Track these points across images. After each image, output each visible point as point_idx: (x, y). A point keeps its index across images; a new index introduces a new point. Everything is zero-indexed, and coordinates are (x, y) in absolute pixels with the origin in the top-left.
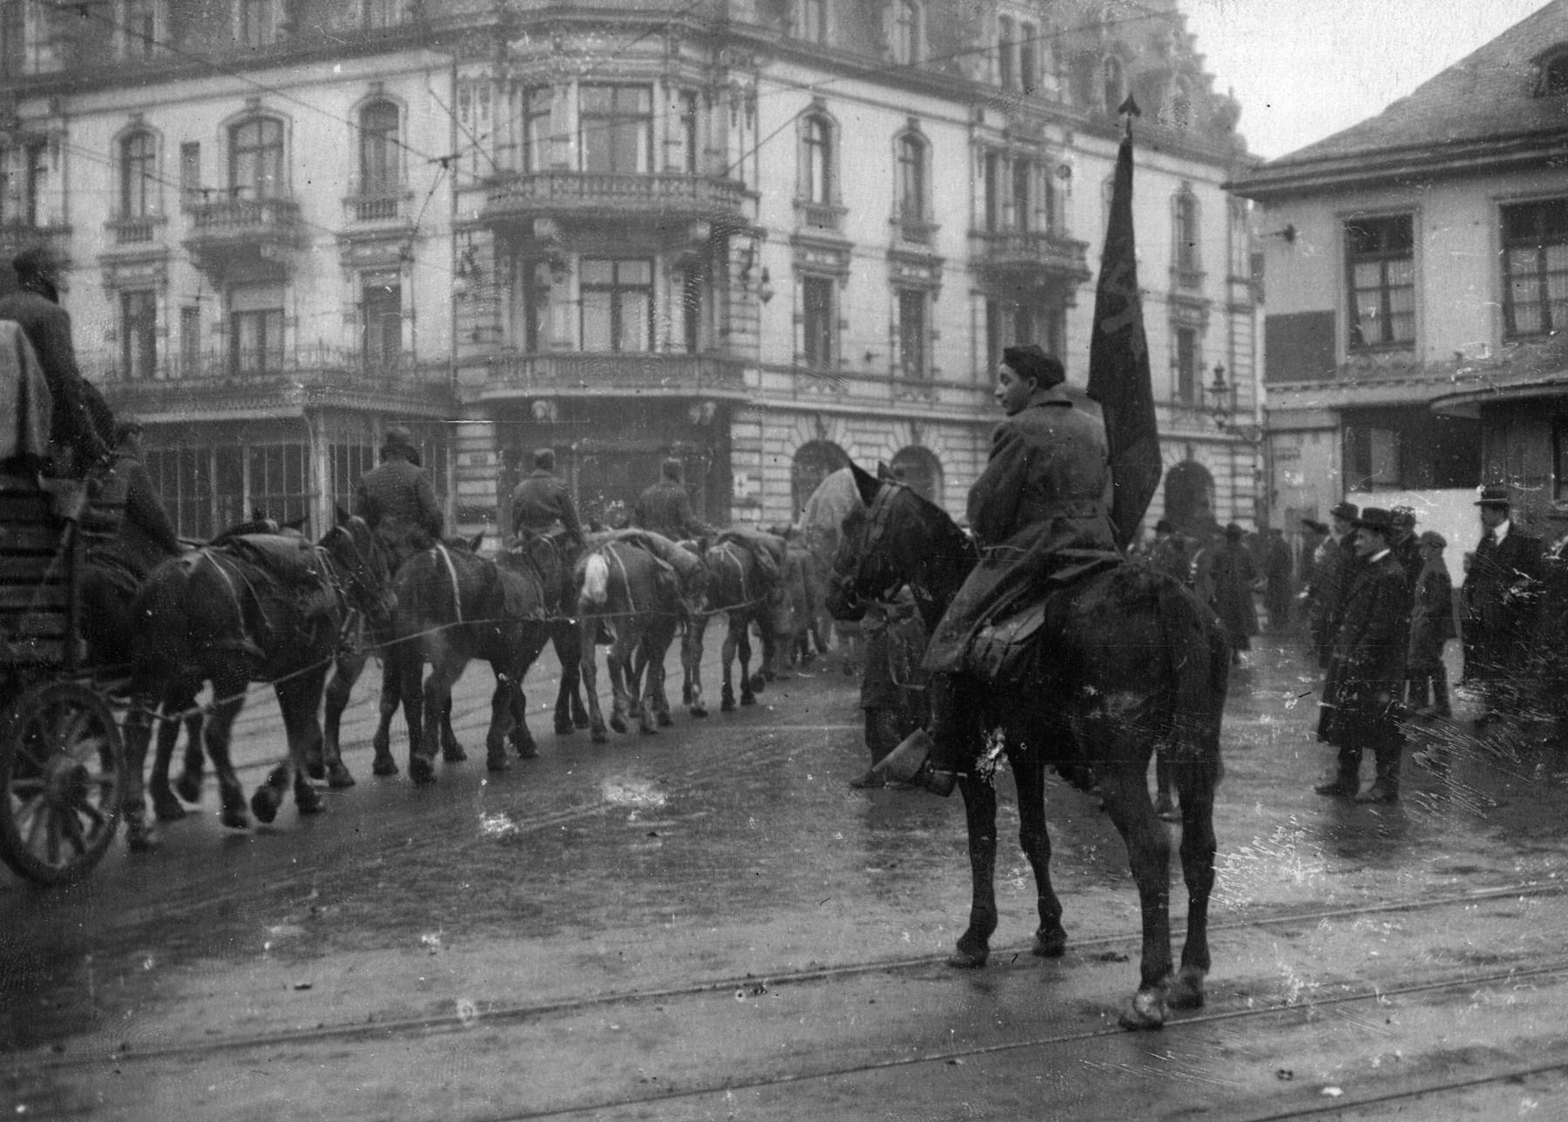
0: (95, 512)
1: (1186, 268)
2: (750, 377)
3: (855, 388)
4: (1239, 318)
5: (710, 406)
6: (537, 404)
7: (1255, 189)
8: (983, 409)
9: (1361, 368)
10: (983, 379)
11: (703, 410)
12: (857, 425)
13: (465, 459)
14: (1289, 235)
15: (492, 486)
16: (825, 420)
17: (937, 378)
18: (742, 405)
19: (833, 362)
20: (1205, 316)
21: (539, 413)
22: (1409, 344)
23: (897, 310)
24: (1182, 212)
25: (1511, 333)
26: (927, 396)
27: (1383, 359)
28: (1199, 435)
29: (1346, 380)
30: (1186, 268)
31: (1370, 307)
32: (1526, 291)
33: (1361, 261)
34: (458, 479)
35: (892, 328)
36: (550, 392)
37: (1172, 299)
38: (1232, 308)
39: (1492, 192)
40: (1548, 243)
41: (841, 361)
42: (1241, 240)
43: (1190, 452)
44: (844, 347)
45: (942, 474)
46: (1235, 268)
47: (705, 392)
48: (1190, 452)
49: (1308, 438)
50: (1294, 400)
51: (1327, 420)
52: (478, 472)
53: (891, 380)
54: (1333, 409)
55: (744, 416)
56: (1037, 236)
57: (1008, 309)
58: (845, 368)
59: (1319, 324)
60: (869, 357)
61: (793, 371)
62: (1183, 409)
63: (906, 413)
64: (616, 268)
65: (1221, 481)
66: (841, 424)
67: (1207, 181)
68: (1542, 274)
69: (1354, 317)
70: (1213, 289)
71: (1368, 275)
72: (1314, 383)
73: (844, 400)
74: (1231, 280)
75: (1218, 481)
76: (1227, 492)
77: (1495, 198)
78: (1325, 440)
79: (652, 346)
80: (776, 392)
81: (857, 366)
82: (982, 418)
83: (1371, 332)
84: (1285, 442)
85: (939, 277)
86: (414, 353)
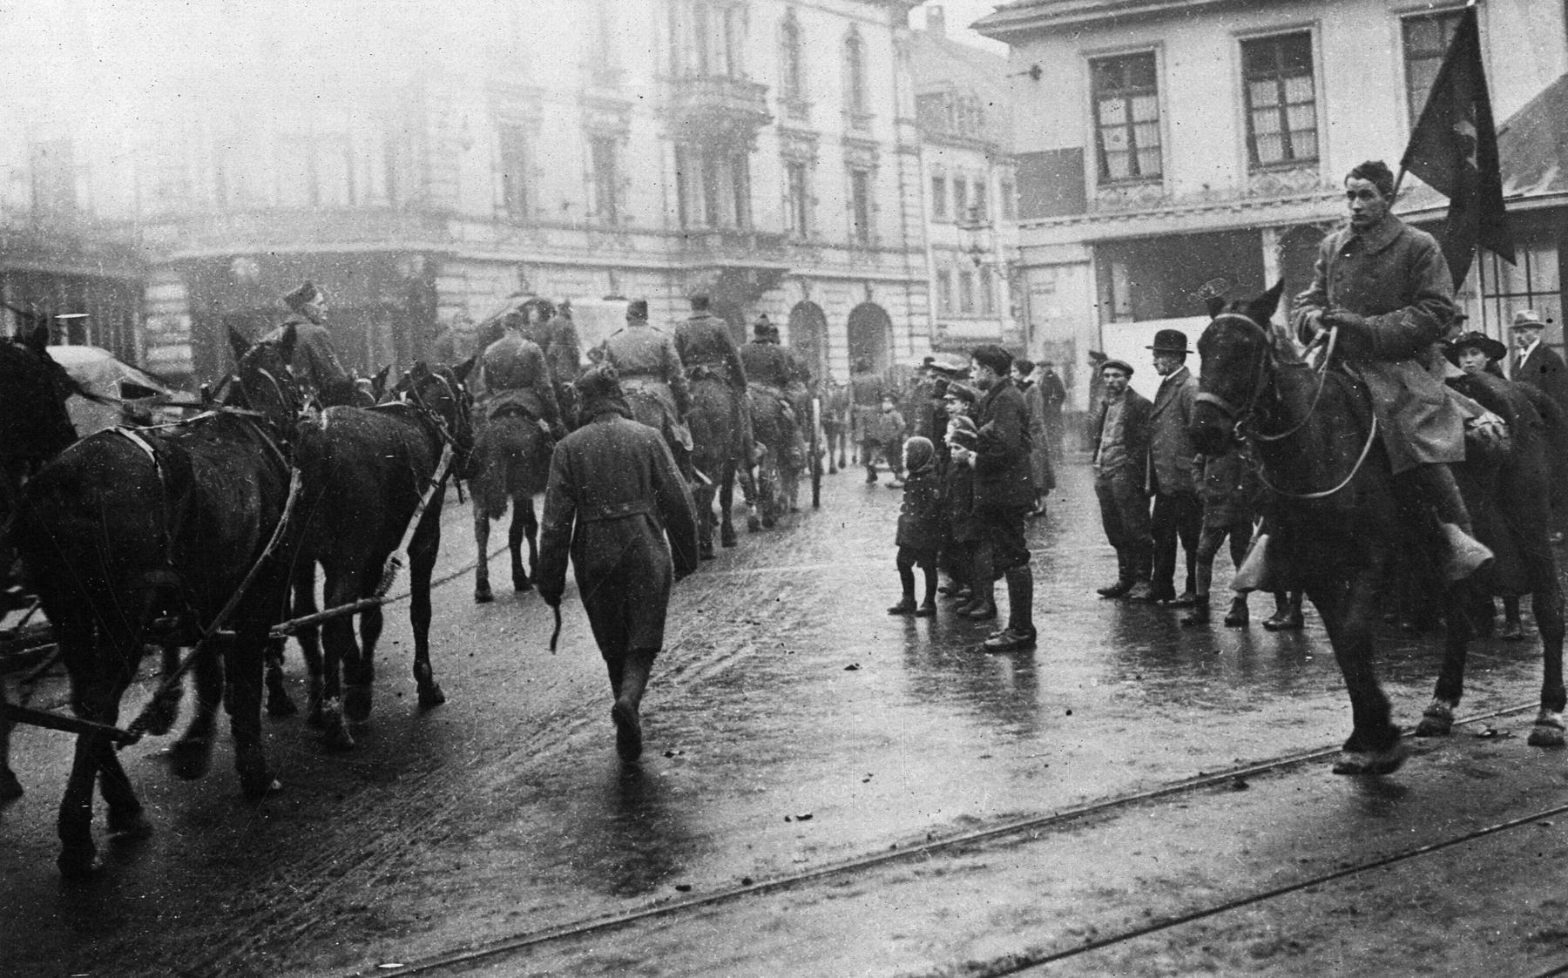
0: (917, 428)
1: (857, 114)
2: (454, 228)
3: (554, 237)
4: (907, 158)
5: (420, 259)
6: (237, 261)
7: (1001, 29)
8: (680, 255)
9: (1112, 203)
10: (676, 226)
11: (412, 265)
12: (557, 276)
13: (154, 324)
14: (1036, 73)
15: (187, 352)
16: (527, 271)
17: (632, 225)
18: (451, 258)
19: (531, 211)
20: (876, 157)
21: (240, 272)
22: (1157, 178)
23: (589, 156)
24: (849, 54)
25: (1255, 163)
26: (622, 244)
27: (1134, 193)
28: (814, 272)
29: (1097, 215)
30: (857, 114)
31: (1117, 141)
32: (1268, 122)
33: (1106, 98)
34: (148, 345)
35: (586, 175)
36: (252, 249)
37: (846, 141)
38: (901, 150)
39: (1230, 26)
40: (1287, 76)
41: (538, 210)
42: (906, 82)
43: (869, 293)
44: (542, 193)
45: (891, 326)
46: (902, 110)
47: (410, 245)
48: (869, 293)
49: (1062, 271)
50: (1048, 236)
51: (1081, 254)
52: (169, 336)
53: (587, 229)
54: (1086, 243)
55: (447, 269)
56: (720, 79)
57: (694, 154)
58: (543, 218)
59: (1073, 159)
60: (566, 206)
61: (495, 221)
62: (860, 250)
63: (604, 262)
64: (1281, 87)
65: (899, 320)
66: (542, 275)
67: (872, 22)
68: (1283, 106)
69: (1102, 157)
70: (882, 131)
71: (1114, 111)
72: (1066, 218)
73: (545, 250)
74: (898, 122)
75: (894, 320)
76: (906, 332)
77: (1237, 34)
78: (1080, 271)
79: (352, 200)
80: (479, 245)
81: (555, 214)
82: (676, 265)
83: (1119, 167)
84: (1044, 276)
85: (627, 122)
86: (91, 211)
